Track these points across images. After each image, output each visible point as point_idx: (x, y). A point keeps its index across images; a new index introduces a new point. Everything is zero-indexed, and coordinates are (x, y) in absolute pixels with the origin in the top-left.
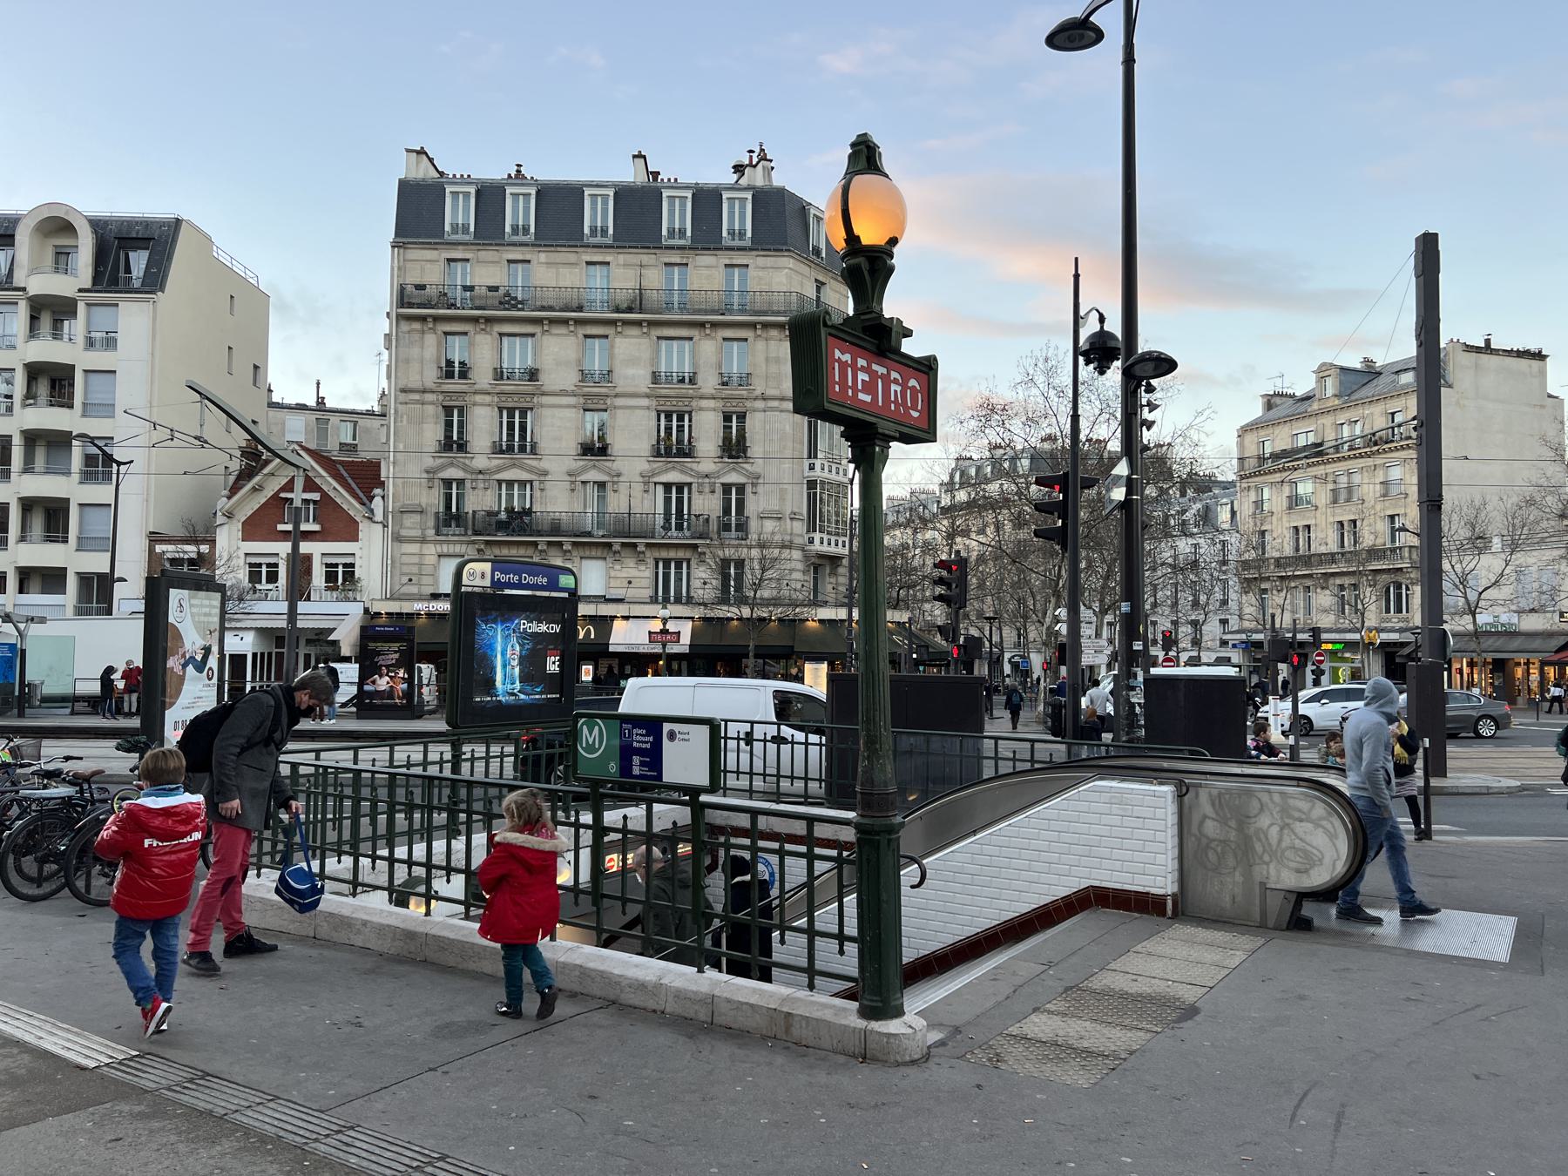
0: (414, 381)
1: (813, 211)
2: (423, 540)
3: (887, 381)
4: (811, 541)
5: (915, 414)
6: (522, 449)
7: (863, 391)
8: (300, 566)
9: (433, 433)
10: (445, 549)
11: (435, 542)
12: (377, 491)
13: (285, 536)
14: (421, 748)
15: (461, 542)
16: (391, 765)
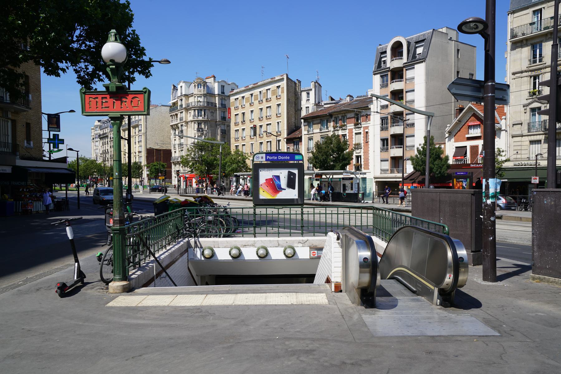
12: (503, 117)
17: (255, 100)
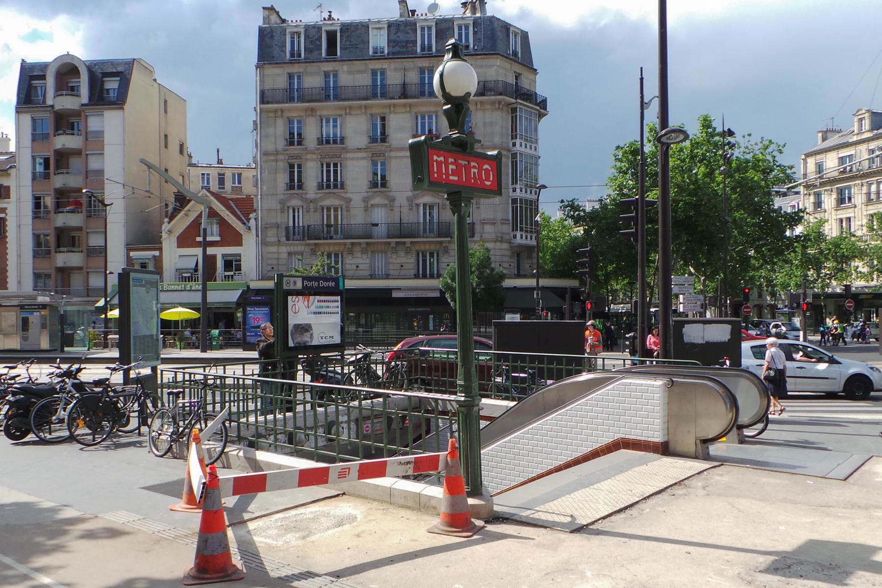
0: (271, 147)
1: (511, 29)
3: (468, 168)
4: (515, 237)
5: (488, 183)
6: (336, 187)
7: (453, 175)
8: (209, 261)
9: (282, 179)
10: (292, 249)
11: (286, 245)
13: (199, 244)
14: (241, 367)
15: (301, 245)
16: (244, 375)
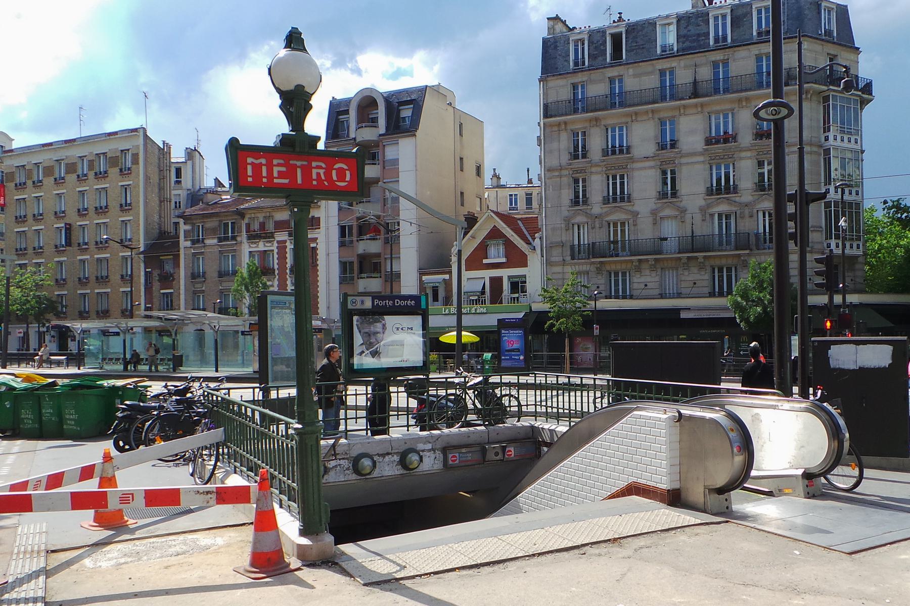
0: (555, 163)
2: (564, 263)
6: (622, 199)
9: (567, 195)
11: (571, 265)
17: (67, 172)
